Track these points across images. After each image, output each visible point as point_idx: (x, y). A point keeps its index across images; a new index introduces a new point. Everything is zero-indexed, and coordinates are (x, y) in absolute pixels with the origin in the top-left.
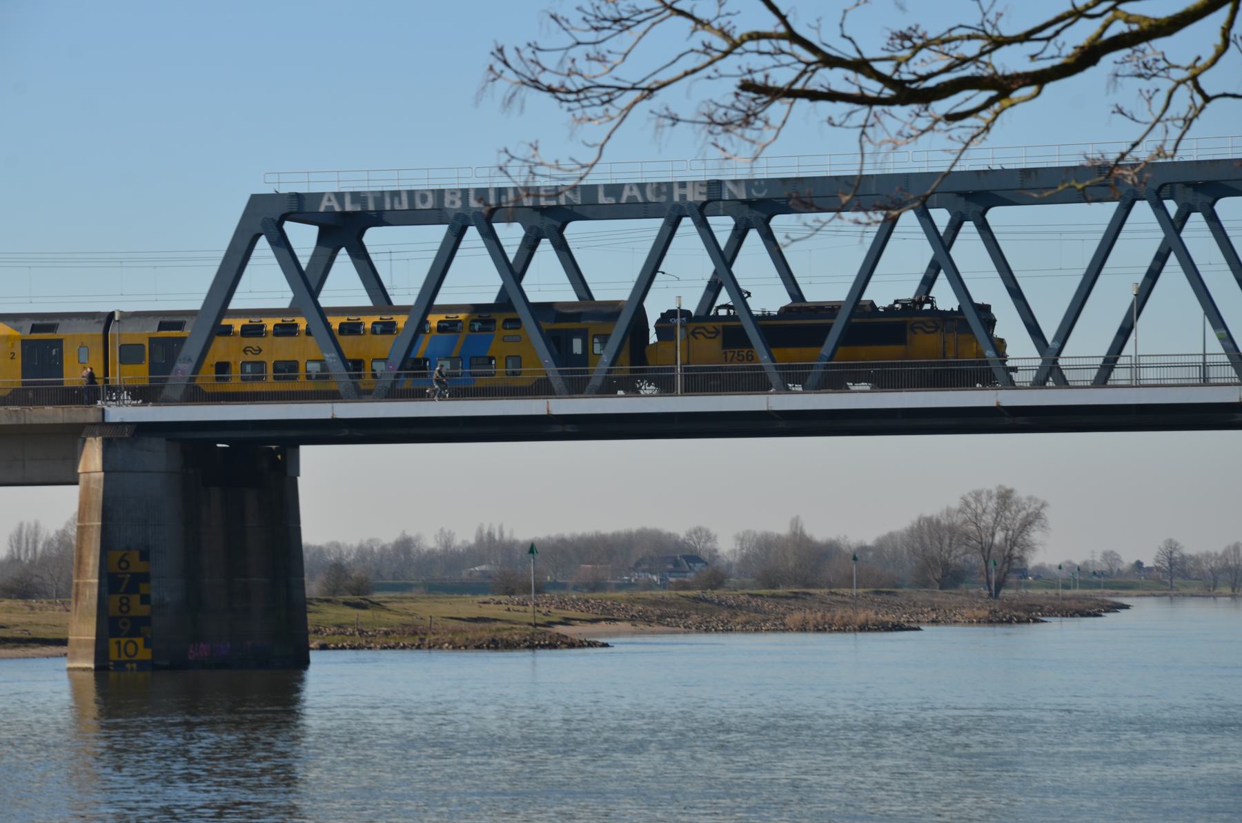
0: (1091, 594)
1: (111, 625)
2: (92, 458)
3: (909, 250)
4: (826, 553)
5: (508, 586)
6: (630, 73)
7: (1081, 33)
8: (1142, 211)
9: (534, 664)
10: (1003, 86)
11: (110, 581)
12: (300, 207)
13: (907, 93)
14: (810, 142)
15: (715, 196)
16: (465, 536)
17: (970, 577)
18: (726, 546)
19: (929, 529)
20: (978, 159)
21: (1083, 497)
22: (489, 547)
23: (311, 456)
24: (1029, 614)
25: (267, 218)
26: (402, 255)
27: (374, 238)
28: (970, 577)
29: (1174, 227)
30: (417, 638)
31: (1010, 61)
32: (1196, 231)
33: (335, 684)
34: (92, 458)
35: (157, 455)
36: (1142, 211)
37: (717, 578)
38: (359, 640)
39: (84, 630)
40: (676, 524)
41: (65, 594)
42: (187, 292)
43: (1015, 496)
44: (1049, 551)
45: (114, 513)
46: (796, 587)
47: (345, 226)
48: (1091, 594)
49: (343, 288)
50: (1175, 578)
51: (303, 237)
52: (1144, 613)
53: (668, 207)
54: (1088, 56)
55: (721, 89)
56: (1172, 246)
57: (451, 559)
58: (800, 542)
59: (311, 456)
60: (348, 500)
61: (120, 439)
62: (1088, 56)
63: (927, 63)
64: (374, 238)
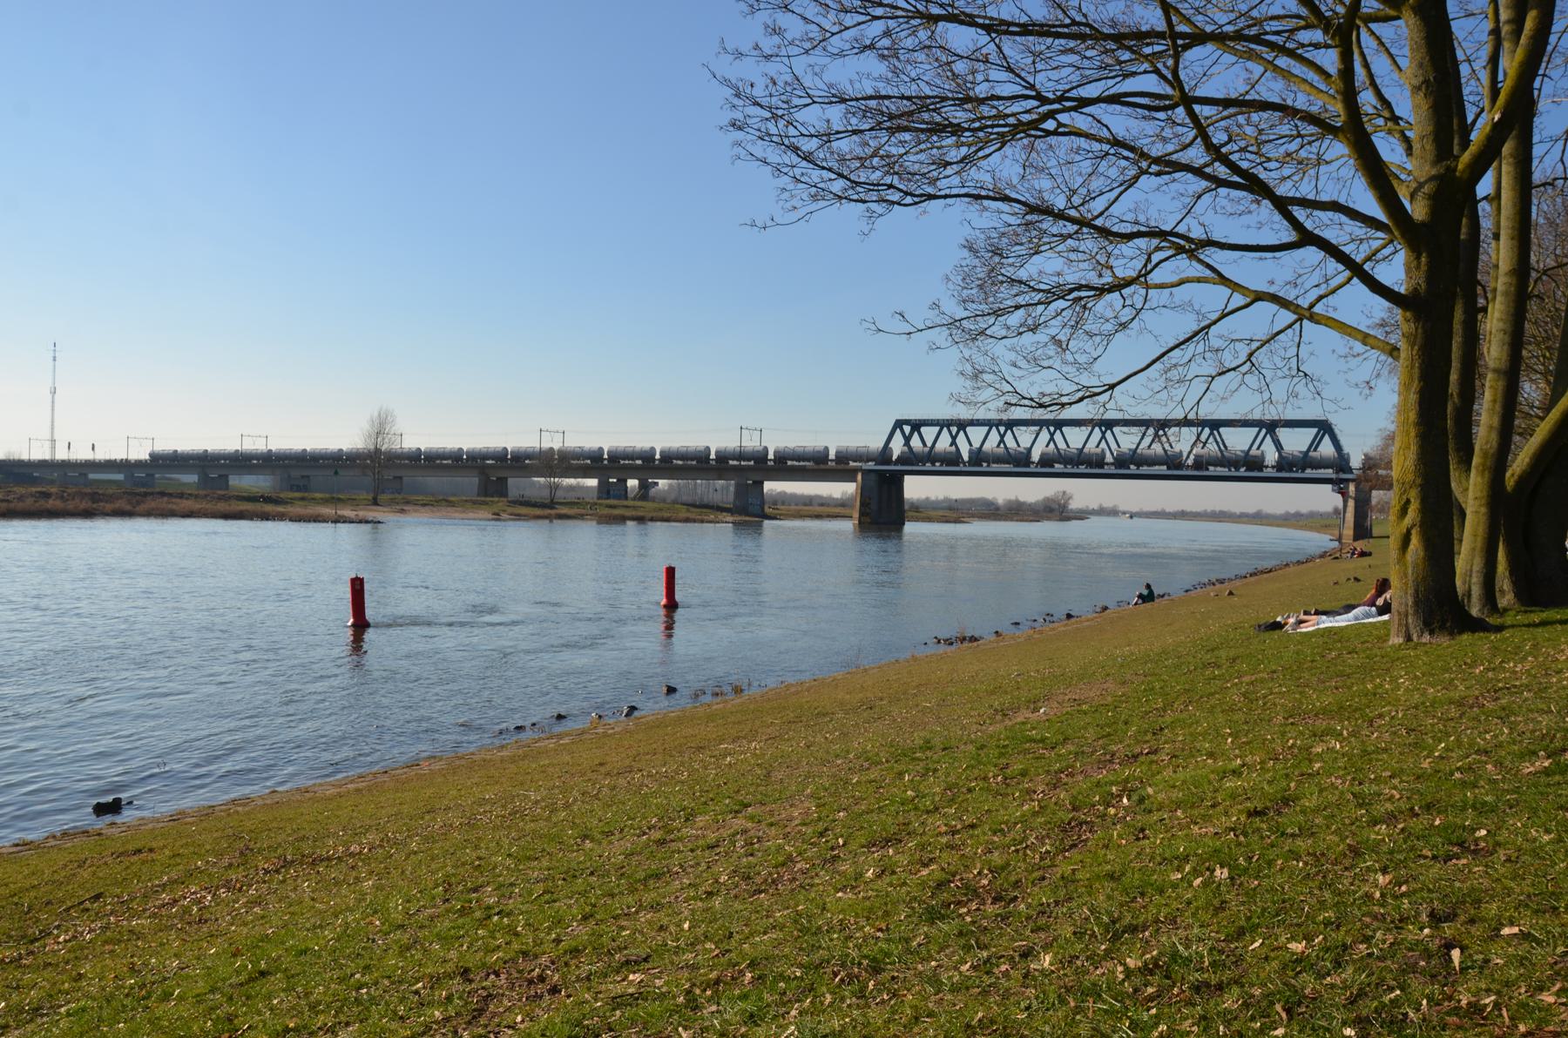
0: (1081, 515)
1: (862, 514)
2: (859, 477)
3: (994, 436)
4: (1024, 504)
5: (950, 509)
6: (980, 399)
7: (1080, 394)
8: (1045, 430)
9: (377, 626)
10: (1063, 405)
11: (862, 504)
12: (907, 422)
13: (1041, 406)
14: (1018, 413)
15: (999, 423)
16: (941, 497)
17: (1055, 510)
18: (1000, 501)
19: (1047, 499)
20: (1061, 417)
21: (1083, 492)
22: (947, 500)
23: (907, 478)
24: (1068, 519)
25: (899, 424)
26: (929, 433)
27: (923, 429)
28: (1055, 510)
29: (1104, 433)
30: (929, 519)
31: (1065, 400)
32: (1108, 434)
33: (910, 528)
34: (859, 477)
35: (873, 477)
36: (1045, 430)
37: (998, 509)
38: (917, 520)
39: (856, 515)
40: (989, 496)
41: (852, 507)
42: (876, 444)
43: (1372, 453)
44: (1074, 505)
45: (863, 490)
46: (1016, 511)
47: (917, 426)
48: (1081, 515)
49: (915, 442)
50: (1101, 512)
51: (907, 429)
52: (1094, 519)
53: (990, 424)
54: (1081, 399)
55: (1000, 404)
56: (1103, 437)
57: (937, 502)
58: (1017, 501)
59: (907, 478)
60: (916, 488)
61: (866, 473)
62: (1081, 399)
63: (1046, 400)
64: (968, 429)
